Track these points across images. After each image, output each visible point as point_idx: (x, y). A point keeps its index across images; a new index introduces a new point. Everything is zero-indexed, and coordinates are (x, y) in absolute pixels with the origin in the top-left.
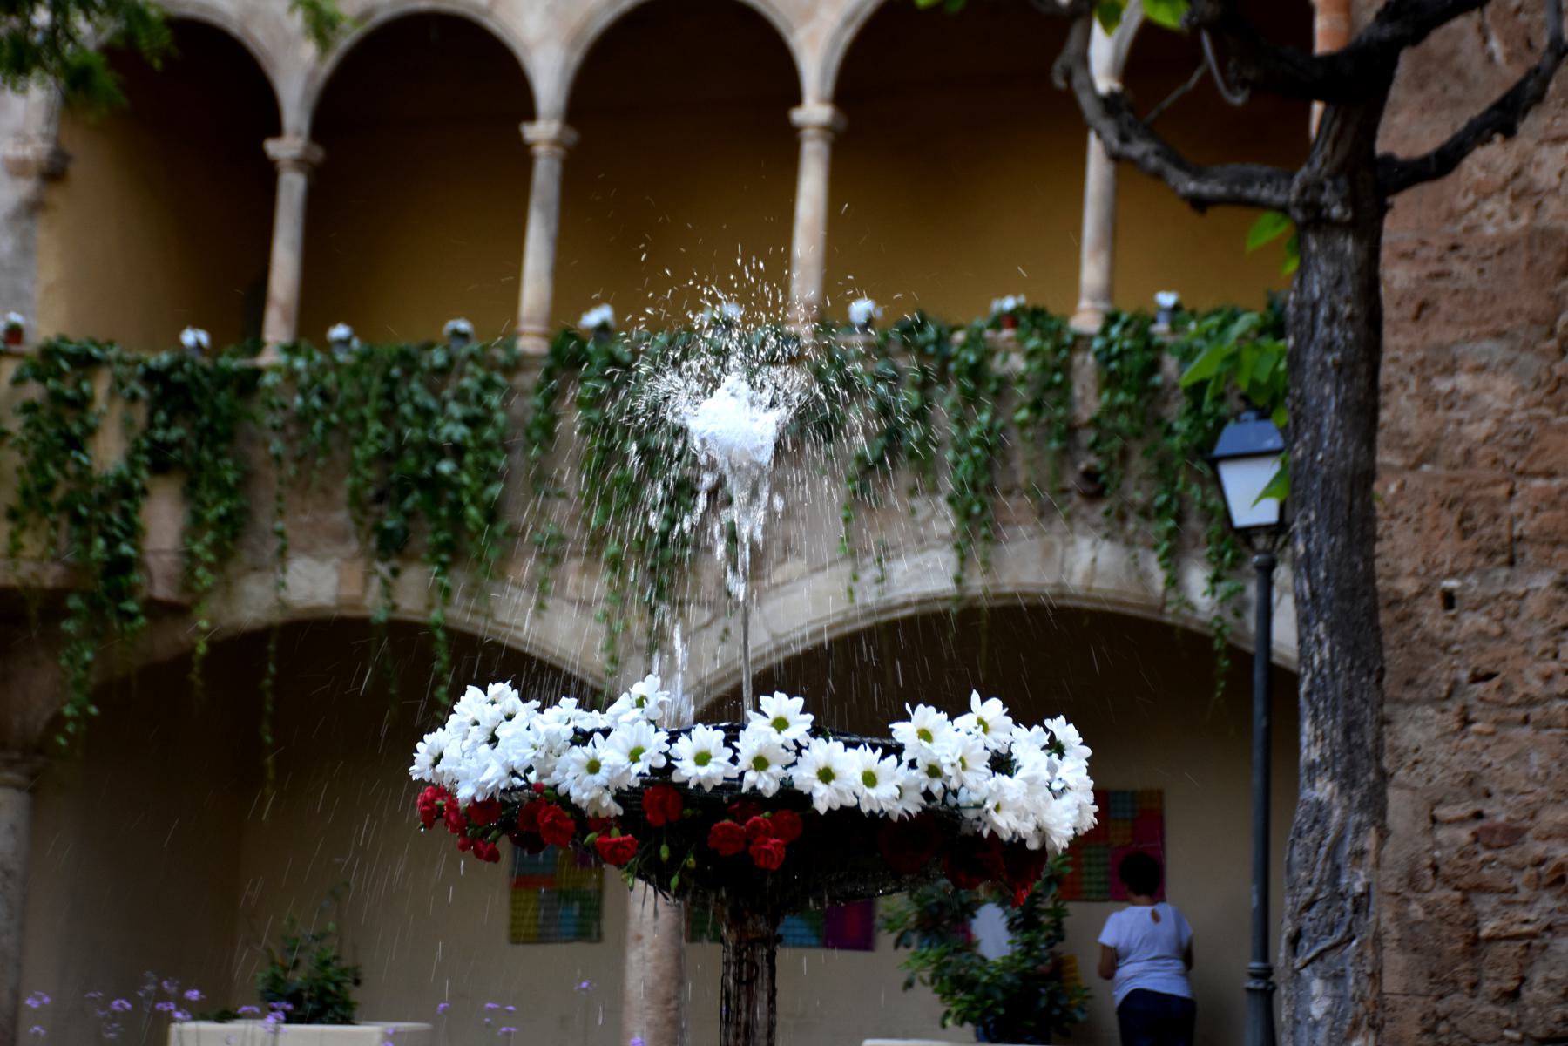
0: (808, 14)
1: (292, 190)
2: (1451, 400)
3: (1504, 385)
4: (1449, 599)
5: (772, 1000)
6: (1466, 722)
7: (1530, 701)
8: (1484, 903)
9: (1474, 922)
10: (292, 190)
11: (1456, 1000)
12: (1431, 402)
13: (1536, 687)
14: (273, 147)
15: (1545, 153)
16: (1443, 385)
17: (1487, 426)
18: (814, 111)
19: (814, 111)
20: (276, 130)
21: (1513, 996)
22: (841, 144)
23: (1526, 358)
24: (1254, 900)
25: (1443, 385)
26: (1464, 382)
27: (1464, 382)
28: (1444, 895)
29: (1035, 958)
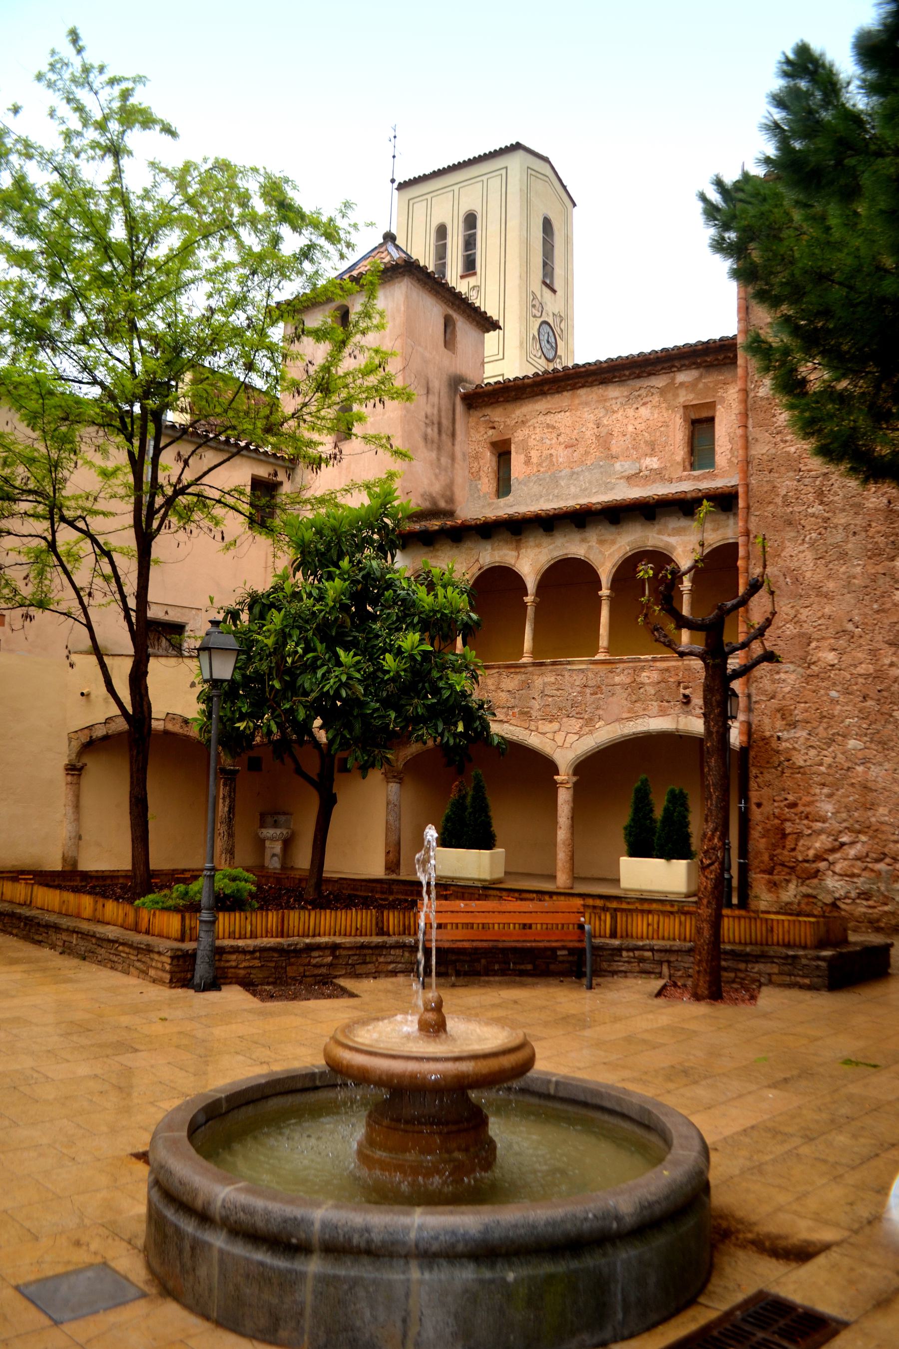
0: (603, 564)
1: (530, 611)
2: (779, 681)
3: (793, 677)
4: (779, 738)
5: (126, 609)
6: (783, 773)
7: (801, 767)
8: (788, 824)
9: (784, 829)
10: (530, 611)
11: (778, 851)
12: (774, 681)
13: (802, 763)
14: (526, 599)
15: (802, 610)
16: (777, 677)
17: (789, 689)
18: (605, 592)
19: (605, 592)
20: (527, 595)
21: (794, 850)
22: (612, 600)
23: (799, 669)
24: (73, 577)
25: (777, 677)
26: (783, 676)
27: (783, 676)
28: (777, 821)
29: (254, 657)
